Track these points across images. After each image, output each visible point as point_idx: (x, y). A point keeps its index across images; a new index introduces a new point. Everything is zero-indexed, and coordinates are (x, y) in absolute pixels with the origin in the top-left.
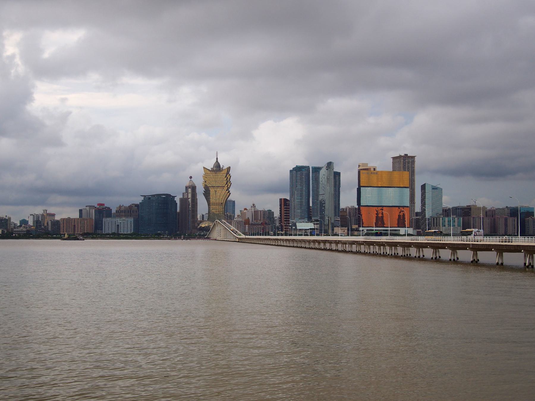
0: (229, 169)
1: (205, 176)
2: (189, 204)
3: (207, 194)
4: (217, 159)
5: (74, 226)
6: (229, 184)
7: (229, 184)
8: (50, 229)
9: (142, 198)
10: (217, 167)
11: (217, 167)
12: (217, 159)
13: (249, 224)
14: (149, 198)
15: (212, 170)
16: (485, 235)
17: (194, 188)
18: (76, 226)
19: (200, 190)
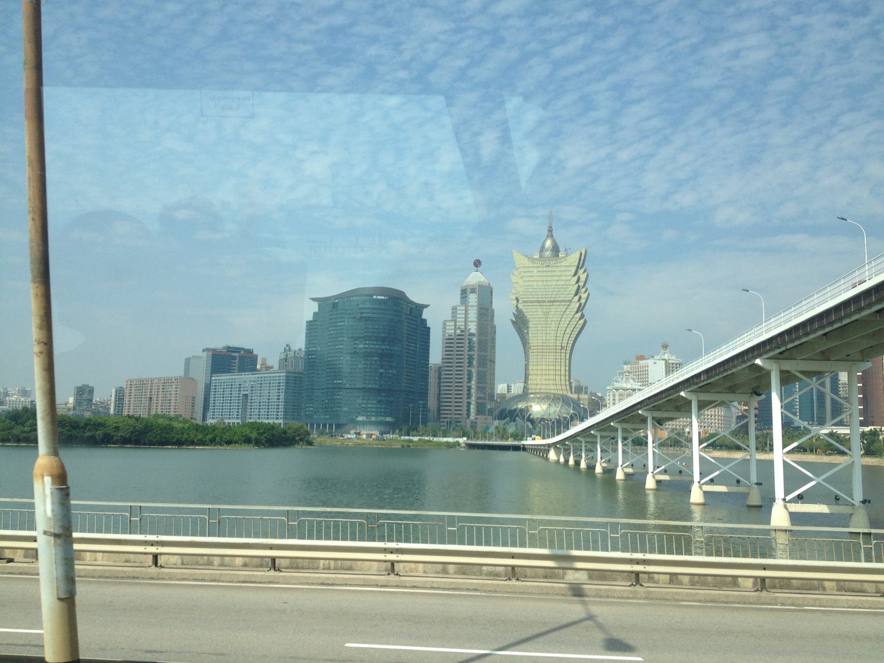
4: (550, 230)
7: (586, 295)
8: (112, 411)
9: (315, 307)
12: (550, 230)
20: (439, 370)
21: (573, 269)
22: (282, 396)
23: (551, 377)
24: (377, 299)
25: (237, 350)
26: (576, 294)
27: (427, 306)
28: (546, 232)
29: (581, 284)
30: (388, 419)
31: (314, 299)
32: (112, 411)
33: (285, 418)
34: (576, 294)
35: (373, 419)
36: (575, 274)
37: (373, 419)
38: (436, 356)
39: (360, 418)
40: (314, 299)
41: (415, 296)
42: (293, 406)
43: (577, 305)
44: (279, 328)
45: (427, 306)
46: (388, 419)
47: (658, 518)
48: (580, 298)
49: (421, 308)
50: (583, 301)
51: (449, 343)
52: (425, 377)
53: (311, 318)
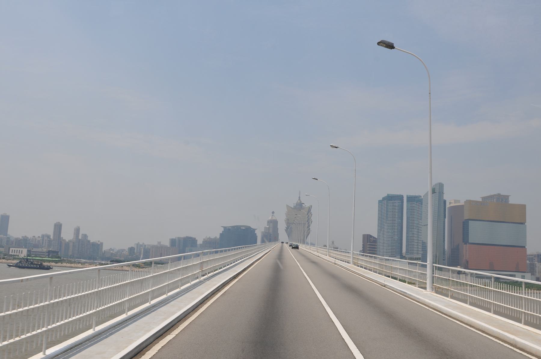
0: (310, 209)
4: (299, 198)
9: (223, 229)
10: (300, 206)
11: (300, 206)
12: (299, 198)
15: (295, 208)
25: (191, 238)
49: (254, 230)
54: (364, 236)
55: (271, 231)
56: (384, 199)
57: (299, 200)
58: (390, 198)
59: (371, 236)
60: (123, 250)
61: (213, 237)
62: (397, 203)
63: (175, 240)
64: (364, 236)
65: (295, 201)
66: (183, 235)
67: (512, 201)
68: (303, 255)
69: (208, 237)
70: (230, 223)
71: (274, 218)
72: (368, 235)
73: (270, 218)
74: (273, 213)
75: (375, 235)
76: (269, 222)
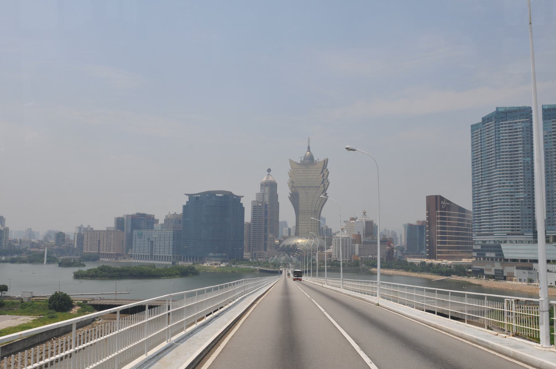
0: (326, 162)
1: (292, 174)
2: (267, 209)
3: (294, 198)
4: (309, 148)
5: (99, 241)
6: (327, 184)
7: (327, 183)
8: (75, 246)
9: (187, 199)
10: (309, 160)
11: (309, 160)
12: (309, 148)
13: (360, 243)
14: (197, 198)
15: (303, 164)
16: (132, 248)
17: (271, 187)
18: (102, 241)
19: (284, 194)
20: (249, 225)
21: (321, 169)
22: (171, 242)
23: (309, 227)
24: (218, 196)
25: (144, 215)
26: (322, 183)
27: (243, 197)
28: (307, 149)
29: (325, 177)
30: (224, 254)
31: (186, 195)
32: (75, 246)
33: (173, 254)
34: (322, 183)
35: (217, 255)
36: (322, 172)
37: (217, 255)
38: (248, 218)
39: (211, 254)
40: (186, 195)
41: (236, 193)
42: (179, 251)
43: (323, 189)
44: (167, 206)
45: (243, 197)
46: (224, 254)
47: (484, 296)
48: (325, 185)
49: (239, 198)
50: (326, 187)
51: (255, 209)
52: (243, 227)
53: (185, 204)
54: (429, 198)
55: (267, 198)
56: (486, 120)
57: (309, 151)
58: (502, 116)
59: (442, 198)
60: (142, 222)
61: (97, 227)
62: (519, 124)
63: (123, 219)
64: (429, 198)
65: (304, 152)
66: (133, 211)
67: (94, 229)
68: (305, 285)
69: (172, 213)
70: (198, 189)
71: (271, 179)
72: (436, 196)
73: (265, 179)
74: (269, 170)
75: (462, 197)
76: (264, 185)
